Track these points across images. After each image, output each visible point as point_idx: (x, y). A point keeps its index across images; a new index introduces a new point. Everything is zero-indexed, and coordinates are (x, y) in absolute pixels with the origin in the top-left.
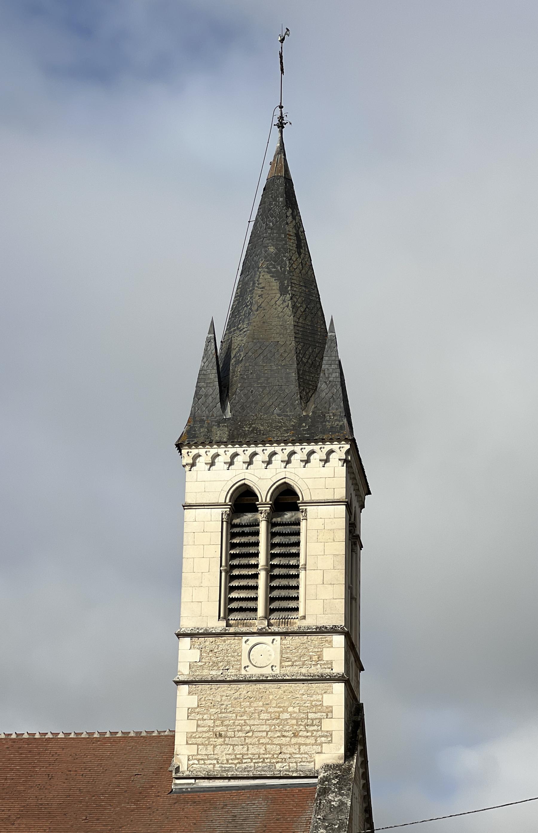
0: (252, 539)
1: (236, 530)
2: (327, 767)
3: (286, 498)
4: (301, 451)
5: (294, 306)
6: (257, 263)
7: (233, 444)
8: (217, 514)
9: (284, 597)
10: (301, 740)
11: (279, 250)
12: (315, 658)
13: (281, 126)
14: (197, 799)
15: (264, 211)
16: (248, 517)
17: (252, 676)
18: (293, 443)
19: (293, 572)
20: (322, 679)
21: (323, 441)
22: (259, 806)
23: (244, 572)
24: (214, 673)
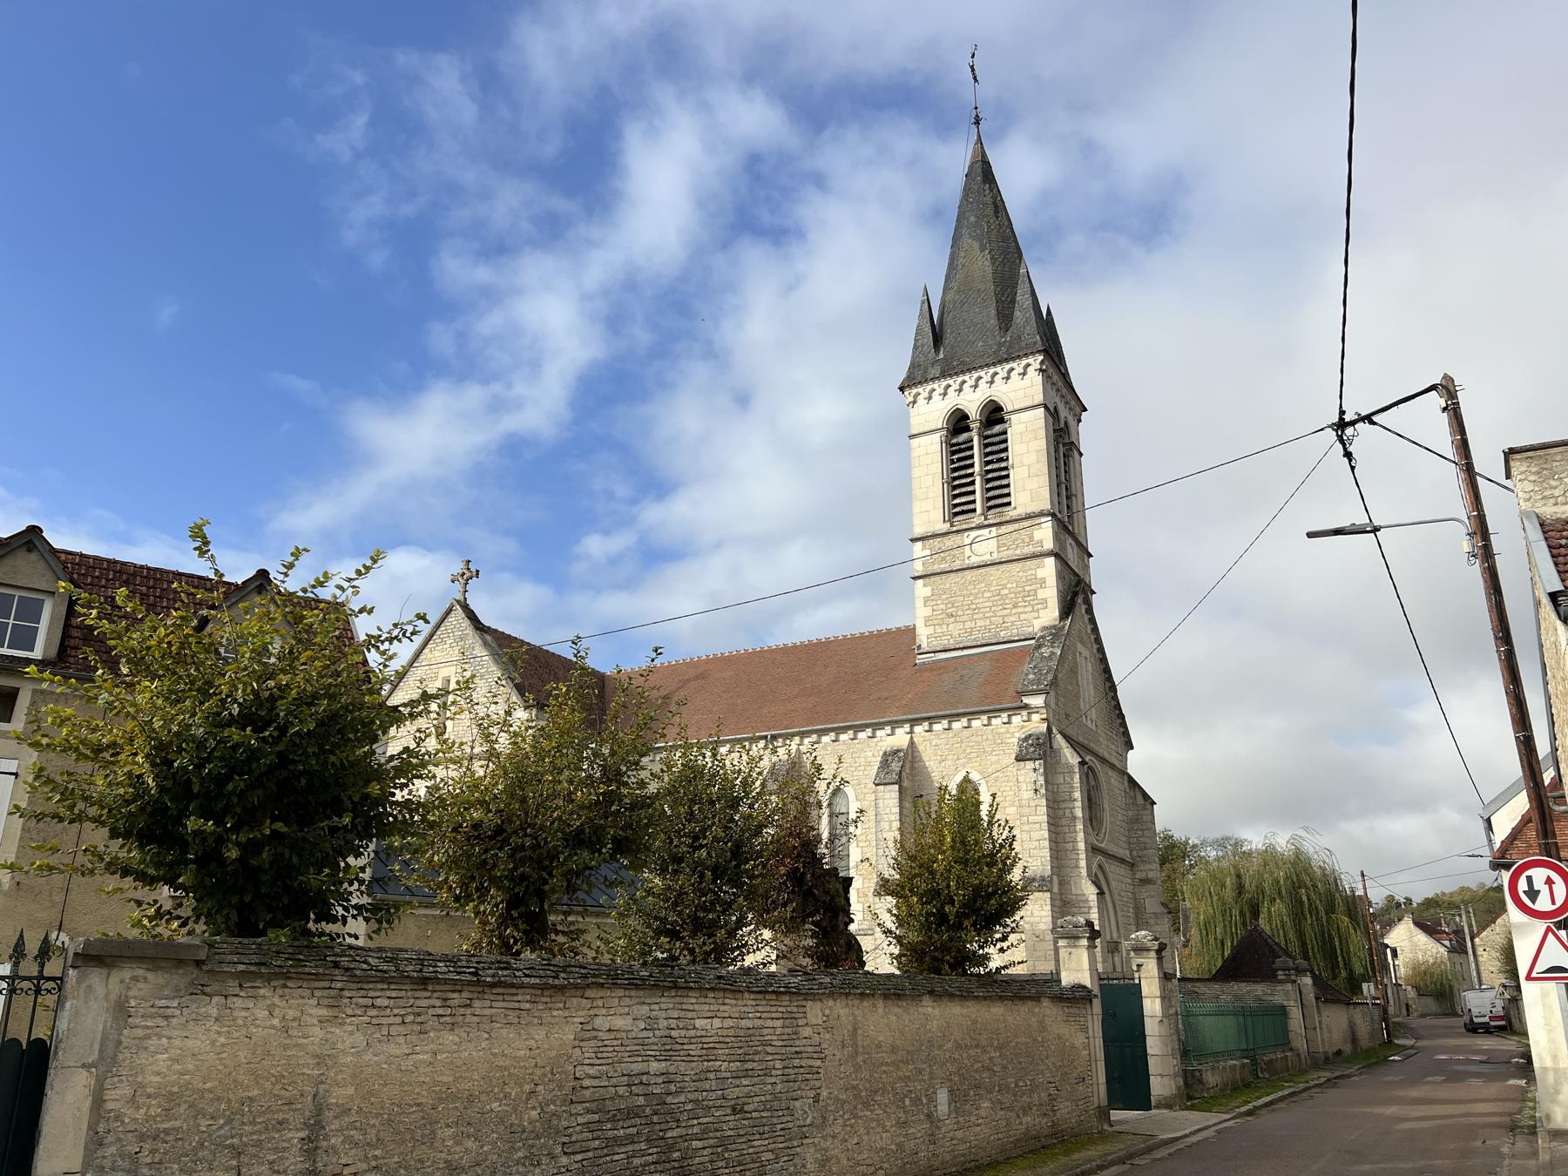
2: (1045, 628)
3: (994, 414)
8: (936, 438)
9: (998, 496)
13: (977, 122)
16: (963, 437)
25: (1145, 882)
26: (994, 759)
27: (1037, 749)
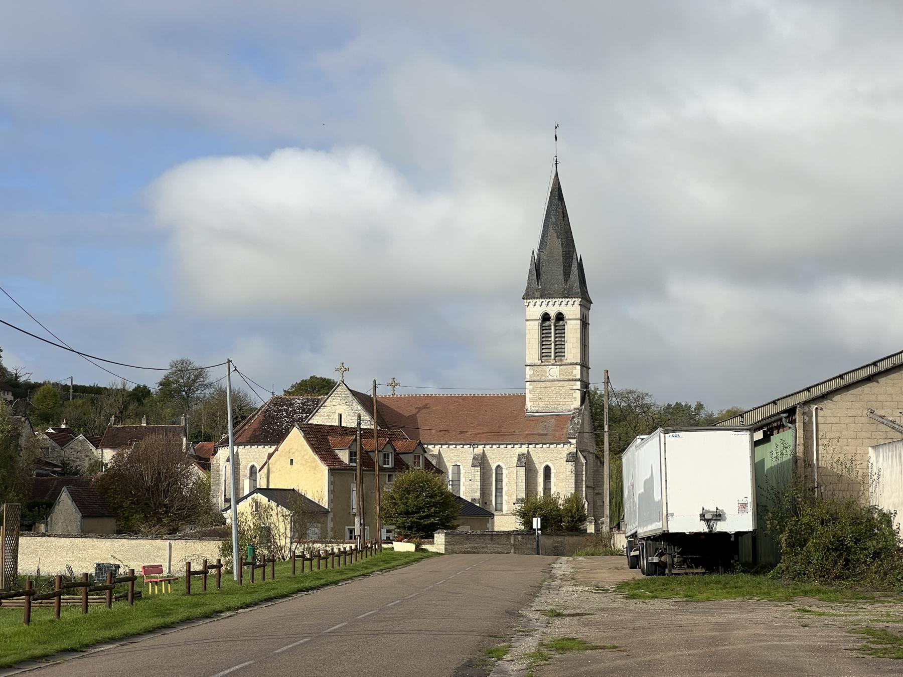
3: (560, 317)
4: (565, 301)
8: (537, 323)
16: (547, 323)
20: (573, 380)
27: (572, 458)
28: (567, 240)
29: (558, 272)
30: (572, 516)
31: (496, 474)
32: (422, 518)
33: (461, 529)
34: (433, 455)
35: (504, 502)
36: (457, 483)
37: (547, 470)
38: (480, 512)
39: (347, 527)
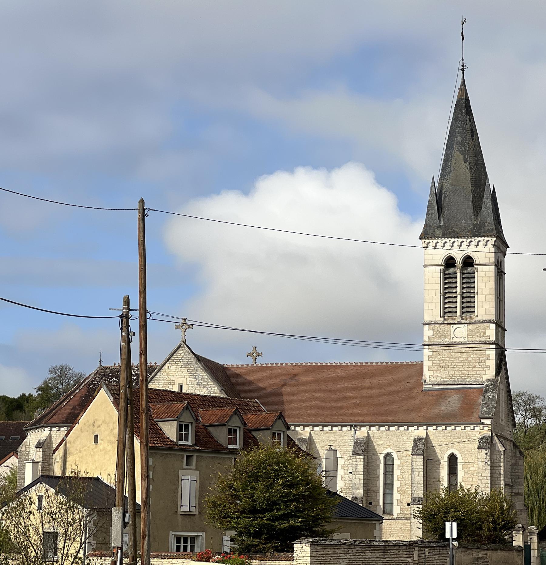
0: (454, 280)
1: (447, 276)
2: (488, 380)
3: (468, 262)
4: (475, 240)
5: (470, 168)
6: (453, 145)
7: (445, 238)
8: (438, 269)
9: (468, 307)
10: (477, 369)
11: (463, 139)
12: (482, 334)
13: (463, 70)
14: (434, 394)
15: (456, 117)
16: (452, 270)
17: (455, 342)
18: (471, 237)
19: (472, 295)
20: (485, 343)
21: (484, 236)
22: (459, 397)
23: (451, 295)
24: (439, 340)
25: (517, 494)
26: (466, 445)
27: (486, 444)
28: (477, 164)
29: (466, 204)
30: (494, 522)
31: (385, 464)
32: (276, 519)
33: (337, 537)
34: (302, 440)
35: (395, 502)
36: (332, 474)
37: (453, 460)
38: (364, 514)
39: (172, 533)
